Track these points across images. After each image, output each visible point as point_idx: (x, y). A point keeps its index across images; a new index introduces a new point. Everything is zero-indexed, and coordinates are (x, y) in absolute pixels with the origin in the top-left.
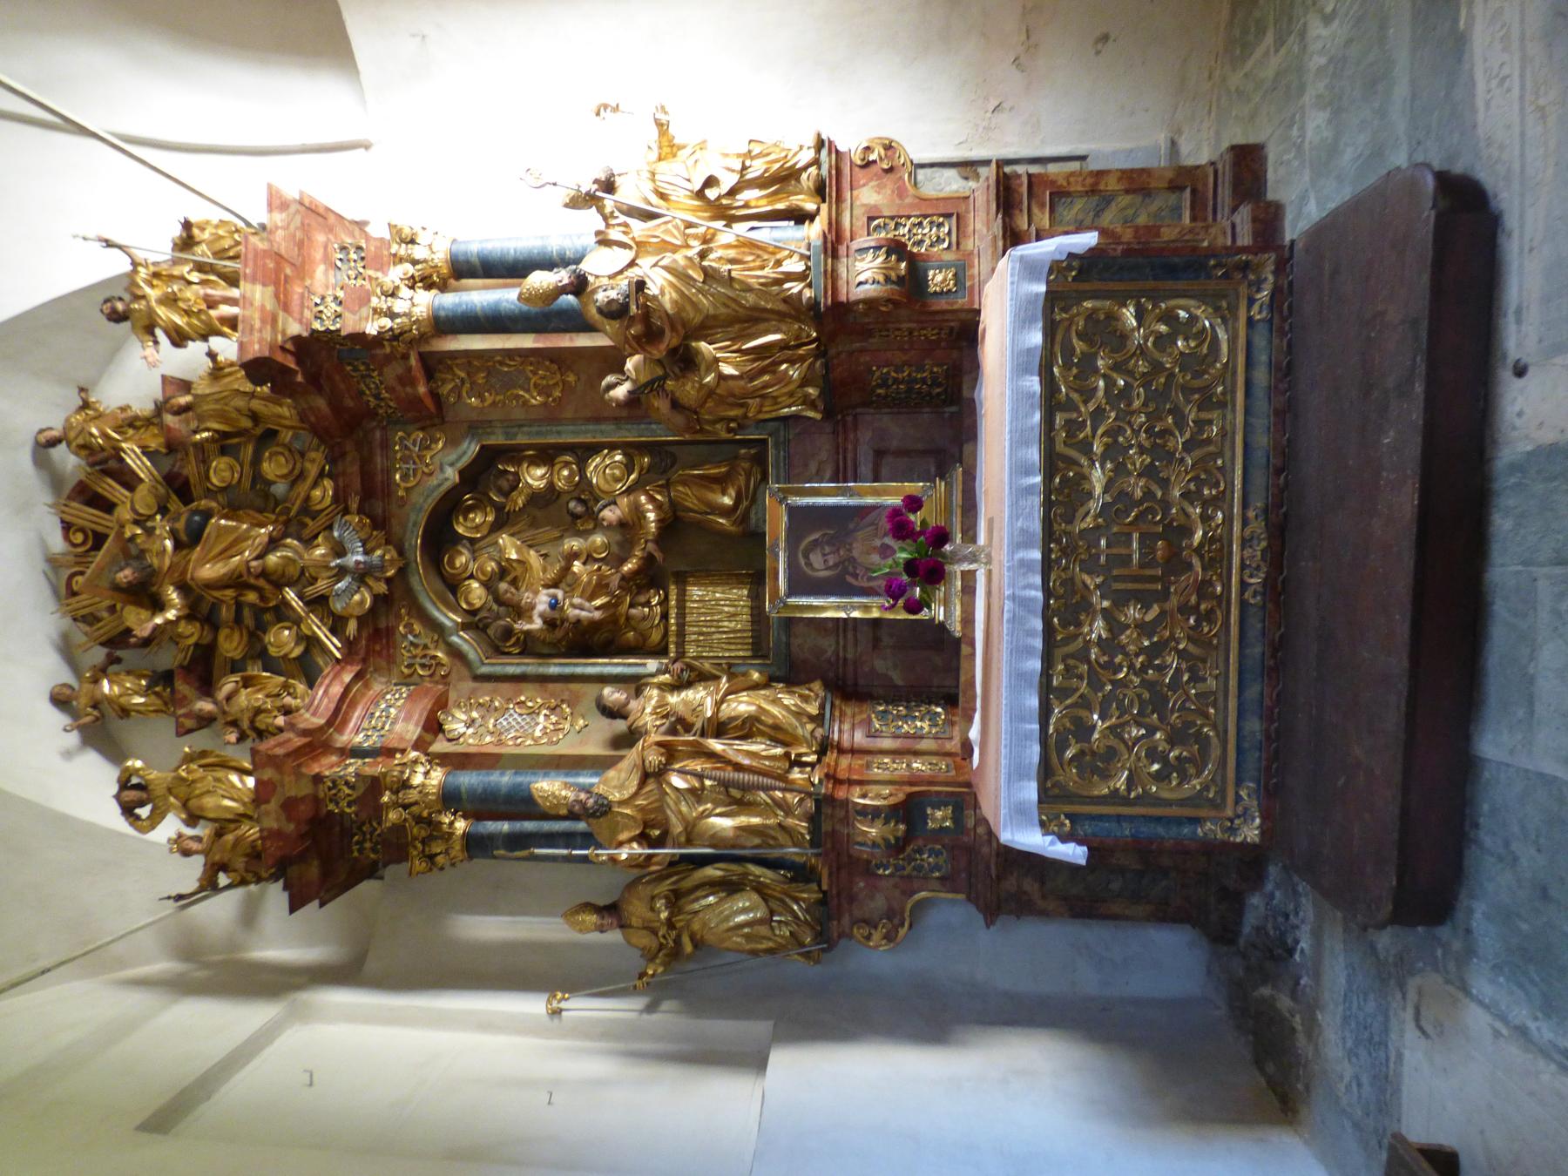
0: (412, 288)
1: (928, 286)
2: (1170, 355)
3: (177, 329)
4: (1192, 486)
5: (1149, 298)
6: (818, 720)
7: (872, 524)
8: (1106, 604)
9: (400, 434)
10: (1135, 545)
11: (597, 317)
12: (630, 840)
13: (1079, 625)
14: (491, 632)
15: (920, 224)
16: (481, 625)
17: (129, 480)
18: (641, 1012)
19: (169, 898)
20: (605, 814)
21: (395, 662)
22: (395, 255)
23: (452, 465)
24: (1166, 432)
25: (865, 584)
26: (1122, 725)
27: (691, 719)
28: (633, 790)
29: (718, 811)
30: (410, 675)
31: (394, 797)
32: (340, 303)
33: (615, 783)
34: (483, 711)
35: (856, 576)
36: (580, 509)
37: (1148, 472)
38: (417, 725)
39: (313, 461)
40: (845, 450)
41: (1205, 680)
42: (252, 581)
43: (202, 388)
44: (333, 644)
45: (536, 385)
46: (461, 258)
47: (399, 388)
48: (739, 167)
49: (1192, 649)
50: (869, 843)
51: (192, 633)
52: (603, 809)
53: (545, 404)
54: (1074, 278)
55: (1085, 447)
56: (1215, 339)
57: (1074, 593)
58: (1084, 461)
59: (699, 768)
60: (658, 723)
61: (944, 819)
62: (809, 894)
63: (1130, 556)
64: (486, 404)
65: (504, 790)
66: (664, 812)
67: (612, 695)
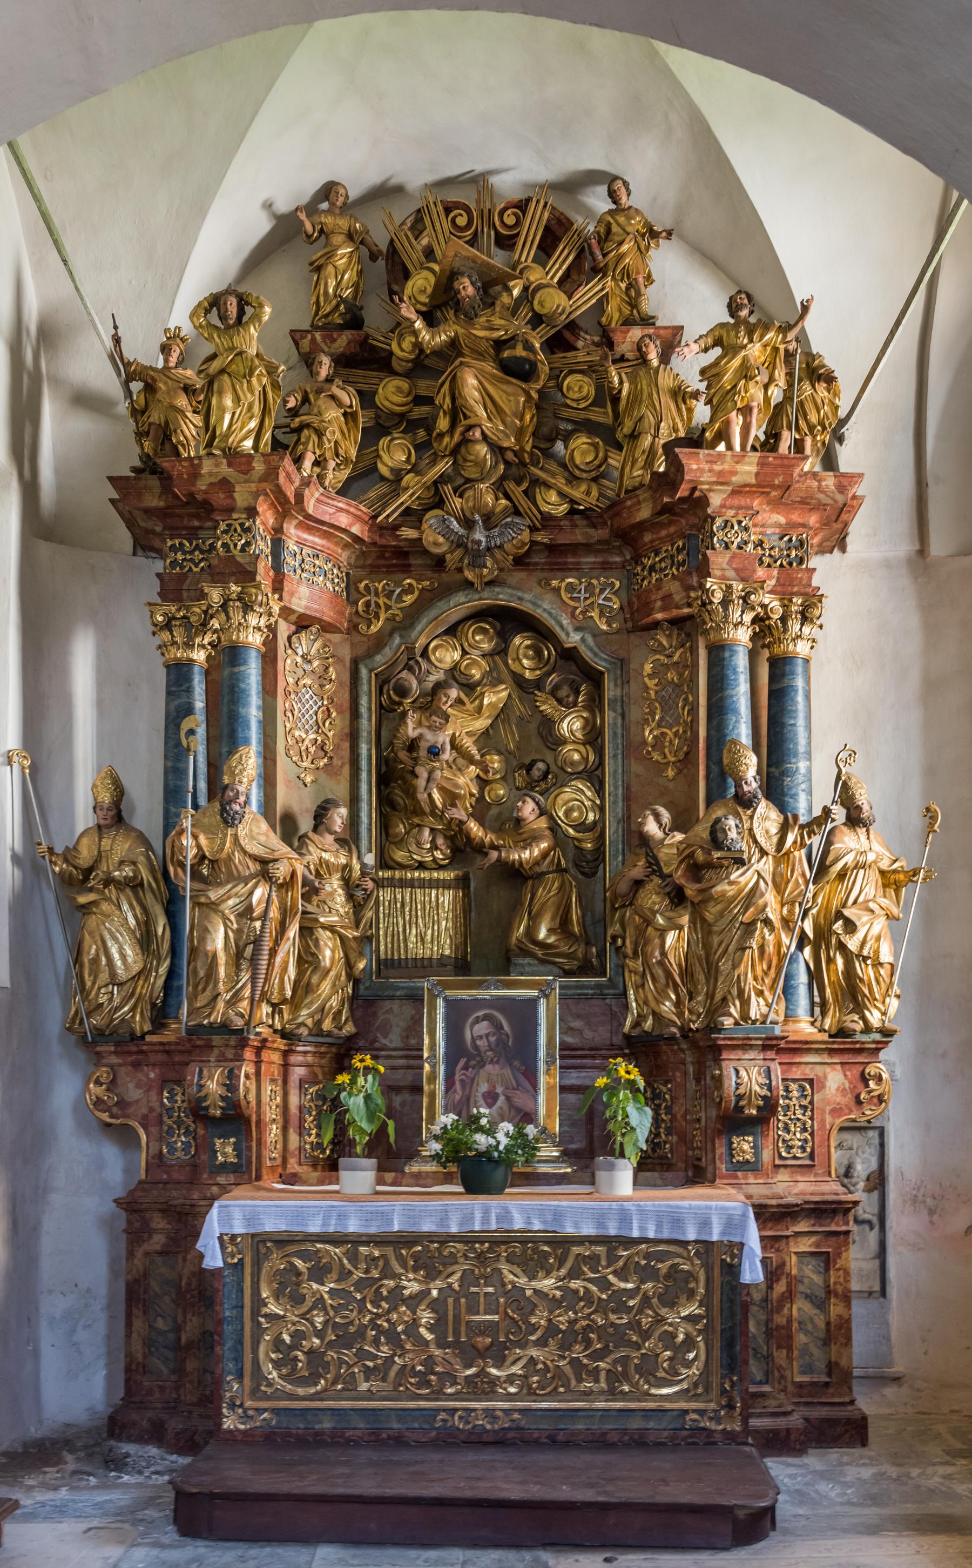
0: (754, 621)
1: (738, 1136)
2: (656, 1345)
3: (719, 376)
4: (540, 1366)
5: (706, 1325)
6: (317, 1030)
7: (518, 1085)
8: (435, 1293)
9: (617, 584)
10: (488, 1317)
11: (714, 817)
12: (199, 847)
13: (415, 1269)
14: (404, 674)
15: (804, 1130)
16: (412, 663)
17: (568, 283)
18: (13, 850)
19: (116, 327)
20: (226, 822)
21: (371, 572)
22: (791, 601)
23: (583, 640)
24: (588, 1343)
25: (457, 1077)
26: (324, 1309)
27: (315, 900)
28: (248, 848)
29: (231, 934)
30: (357, 589)
31: (234, 596)
32: (740, 548)
33: (255, 830)
34: (320, 671)
35: (466, 1068)
36: (536, 773)
37: (552, 1329)
38: (306, 608)
39: (588, 493)
40: (593, 1057)
41: (367, 1380)
42: (459, 430)
43: (665, 380)
44: (391, 512)
45: (663, 734)
46: (788, 668)
47: (661, 594)
48: (865, 953)
49: (395, 1368)
50: (202, 1082)
51: (402, 350)
52: (229, 819)
53: (645, 742)
54: (723, 1261)
55: (575, 1274)
56: (670, 1384)
57: (444, 1265)
58: (563, 1272)
59: (271, 915)
60: (312, 867)
61: (224, 1154)
62: (140, 1023)
63: (478, 1313)
64: (646, 679)
65: (242, 711)
66: (228, 882)
67: (339, 817)
